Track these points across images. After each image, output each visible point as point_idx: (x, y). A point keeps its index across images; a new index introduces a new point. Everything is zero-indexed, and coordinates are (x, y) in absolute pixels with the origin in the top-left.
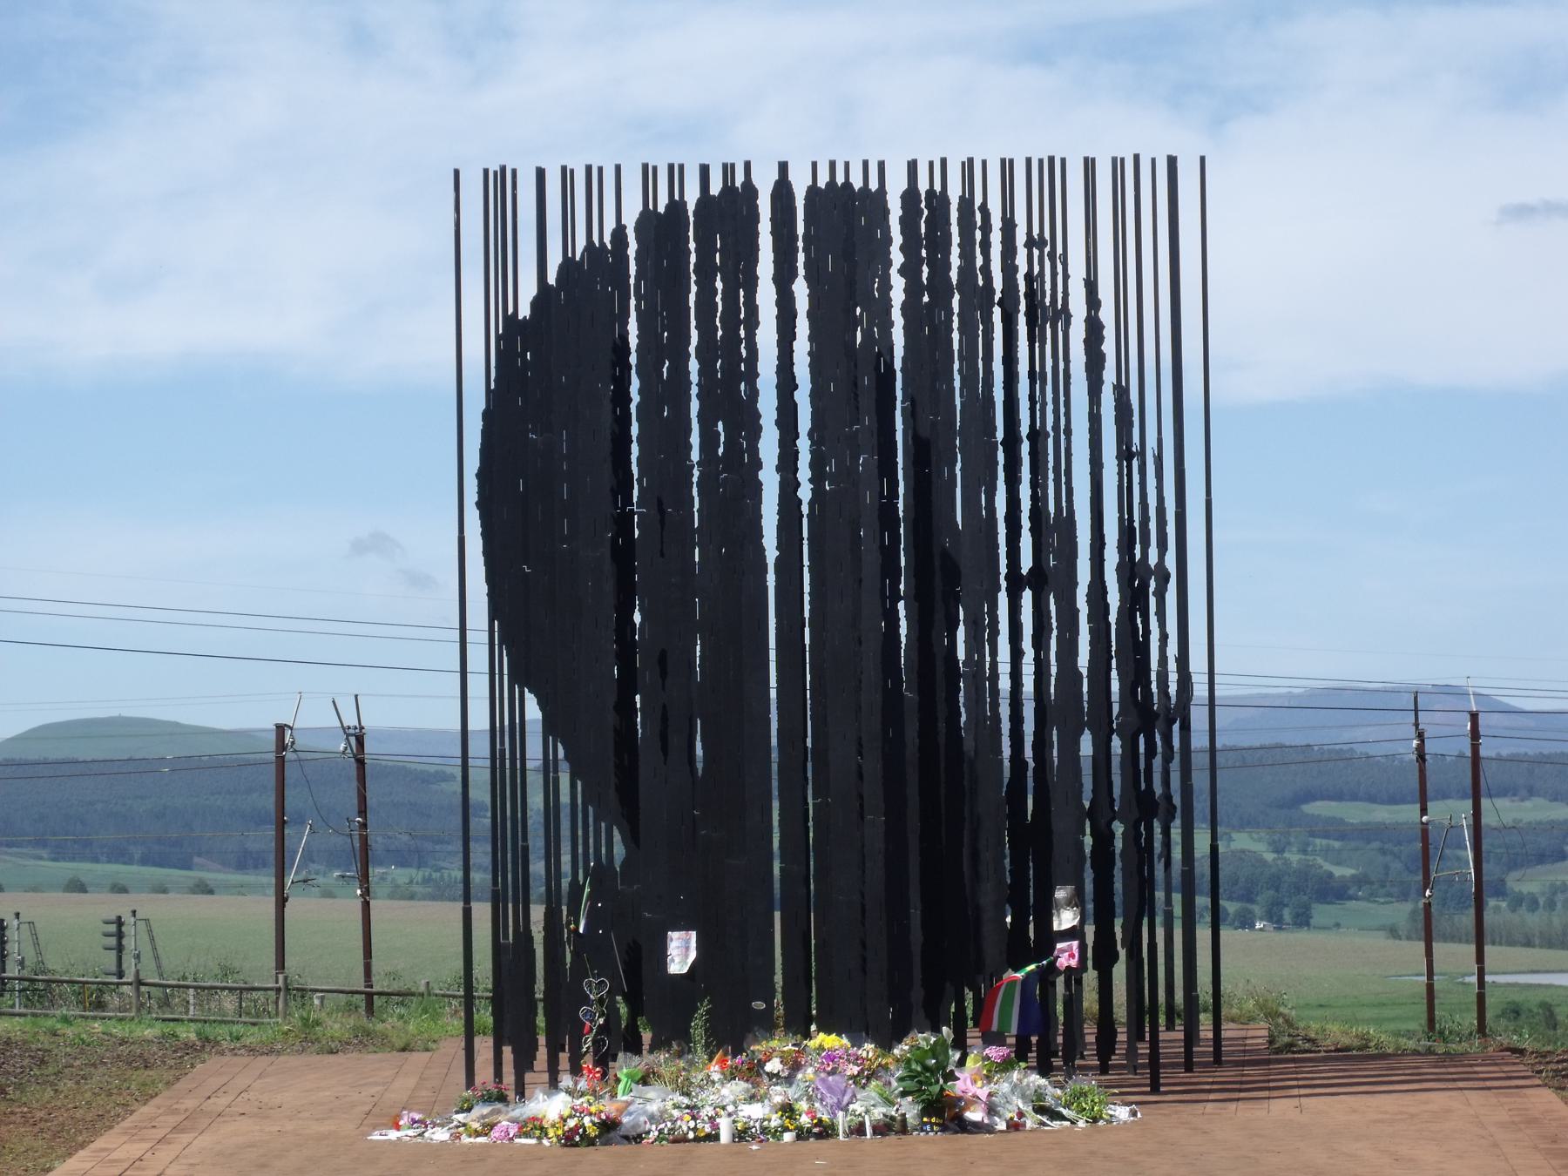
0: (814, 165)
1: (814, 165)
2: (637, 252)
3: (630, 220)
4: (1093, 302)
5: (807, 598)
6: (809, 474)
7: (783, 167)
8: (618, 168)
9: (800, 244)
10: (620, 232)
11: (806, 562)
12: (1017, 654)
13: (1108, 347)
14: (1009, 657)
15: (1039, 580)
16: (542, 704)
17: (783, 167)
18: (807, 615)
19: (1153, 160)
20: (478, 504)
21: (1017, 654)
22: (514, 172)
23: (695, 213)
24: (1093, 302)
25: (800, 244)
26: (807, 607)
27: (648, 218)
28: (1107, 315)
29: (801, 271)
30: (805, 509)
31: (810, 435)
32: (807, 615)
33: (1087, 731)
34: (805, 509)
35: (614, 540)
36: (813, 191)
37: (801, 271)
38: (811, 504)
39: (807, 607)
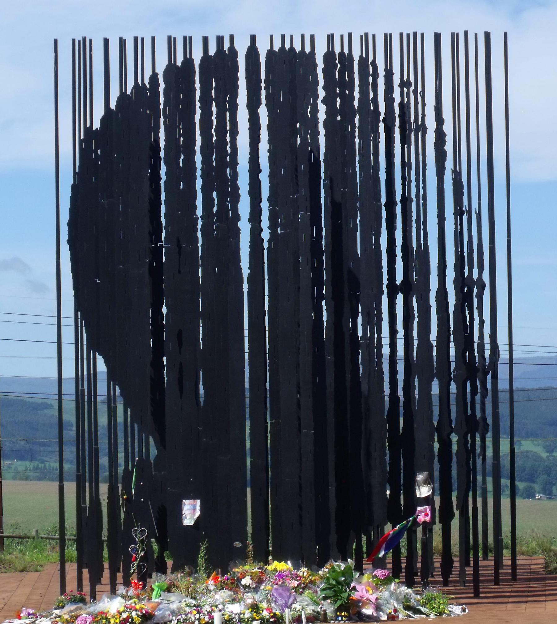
0: (272, 37)
1: (272, 37)
2: (165, 89)
3: (160, 70)
4: (440, 121)
5: (267, 299)
6: (268, 224)
7: (253, 38)
8: (153, 39)
9: (263, 85)
10: (154, 78)
11: (266, 277)
12: (393, 333)
13: (449, 147)
14: (390, 334)
15: (407, 288)
16: (107, 362)
17: (253, 38)
18: (267, 308)
19: (476, 35)
20: (69, 242)
21: (393, 333)
22: (91, 41)
23: (200, 66)
24: (440, 121)
25: (263, 85)
26: (267, 304)
27: (171, 68)
28: (448, 128)
29: (264, 101)
30: (266, 245)
31: (269, 200)
32: (267, 308)
33: (435, 379)
34: (266, 245)
35: (150, 264)
36: (270, 53)
37: (264, 101)
38: (269, 241)
39: (267, 304)
